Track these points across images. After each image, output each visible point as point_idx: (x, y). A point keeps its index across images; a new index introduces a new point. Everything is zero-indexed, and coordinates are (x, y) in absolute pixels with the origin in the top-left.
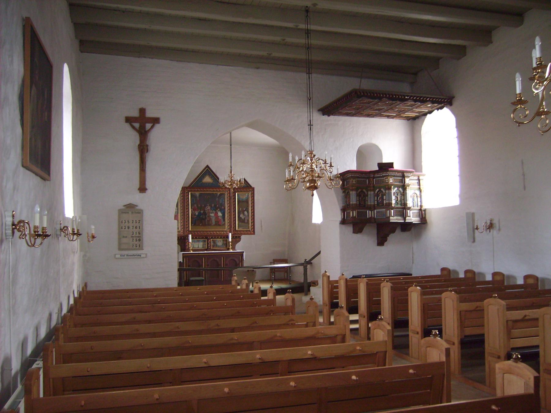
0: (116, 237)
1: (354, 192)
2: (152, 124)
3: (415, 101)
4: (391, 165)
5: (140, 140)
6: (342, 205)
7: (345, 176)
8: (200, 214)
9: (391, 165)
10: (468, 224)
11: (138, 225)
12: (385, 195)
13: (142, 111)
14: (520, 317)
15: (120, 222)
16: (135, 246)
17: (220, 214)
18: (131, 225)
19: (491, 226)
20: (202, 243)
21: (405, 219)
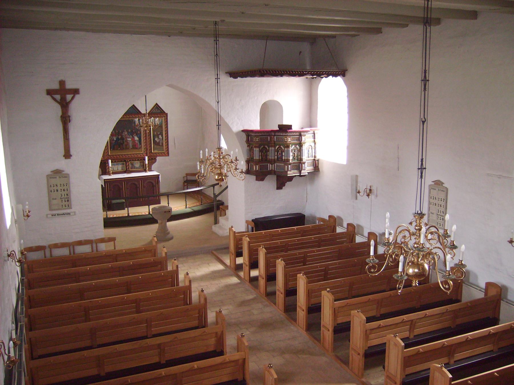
0: (46, 199)
1: (257, 149)
2: (72, 95)
3: (313, 75)
4: (290, 127)
5: (63, 112)
6: (246, 157)
7: (249, 135)
8: (118, 139)
9: (290, 127)
10: (352, 185)
11: (65, 188)
12: (284, 152)
13: (62, 83)
14: (376, 327)
15: (49, 186)
16: (64, 206)
17: (136, 138)
18: (59, 188)
19: (369, 192)
20: (121, 166)
21: (300, 172)
